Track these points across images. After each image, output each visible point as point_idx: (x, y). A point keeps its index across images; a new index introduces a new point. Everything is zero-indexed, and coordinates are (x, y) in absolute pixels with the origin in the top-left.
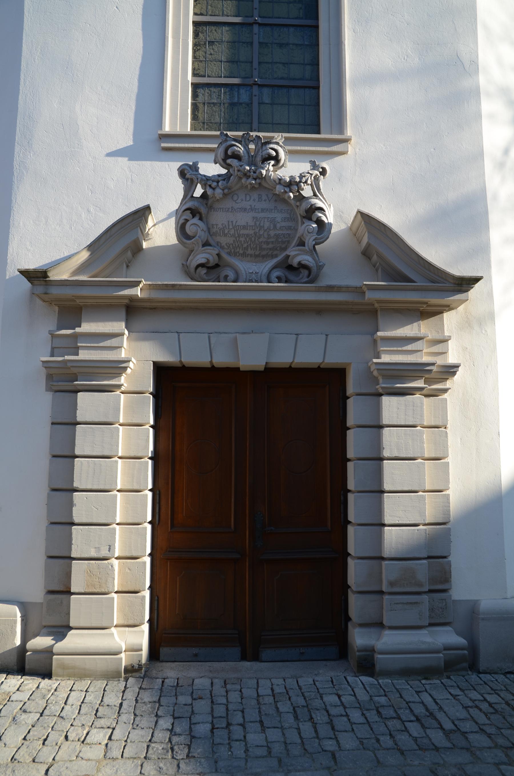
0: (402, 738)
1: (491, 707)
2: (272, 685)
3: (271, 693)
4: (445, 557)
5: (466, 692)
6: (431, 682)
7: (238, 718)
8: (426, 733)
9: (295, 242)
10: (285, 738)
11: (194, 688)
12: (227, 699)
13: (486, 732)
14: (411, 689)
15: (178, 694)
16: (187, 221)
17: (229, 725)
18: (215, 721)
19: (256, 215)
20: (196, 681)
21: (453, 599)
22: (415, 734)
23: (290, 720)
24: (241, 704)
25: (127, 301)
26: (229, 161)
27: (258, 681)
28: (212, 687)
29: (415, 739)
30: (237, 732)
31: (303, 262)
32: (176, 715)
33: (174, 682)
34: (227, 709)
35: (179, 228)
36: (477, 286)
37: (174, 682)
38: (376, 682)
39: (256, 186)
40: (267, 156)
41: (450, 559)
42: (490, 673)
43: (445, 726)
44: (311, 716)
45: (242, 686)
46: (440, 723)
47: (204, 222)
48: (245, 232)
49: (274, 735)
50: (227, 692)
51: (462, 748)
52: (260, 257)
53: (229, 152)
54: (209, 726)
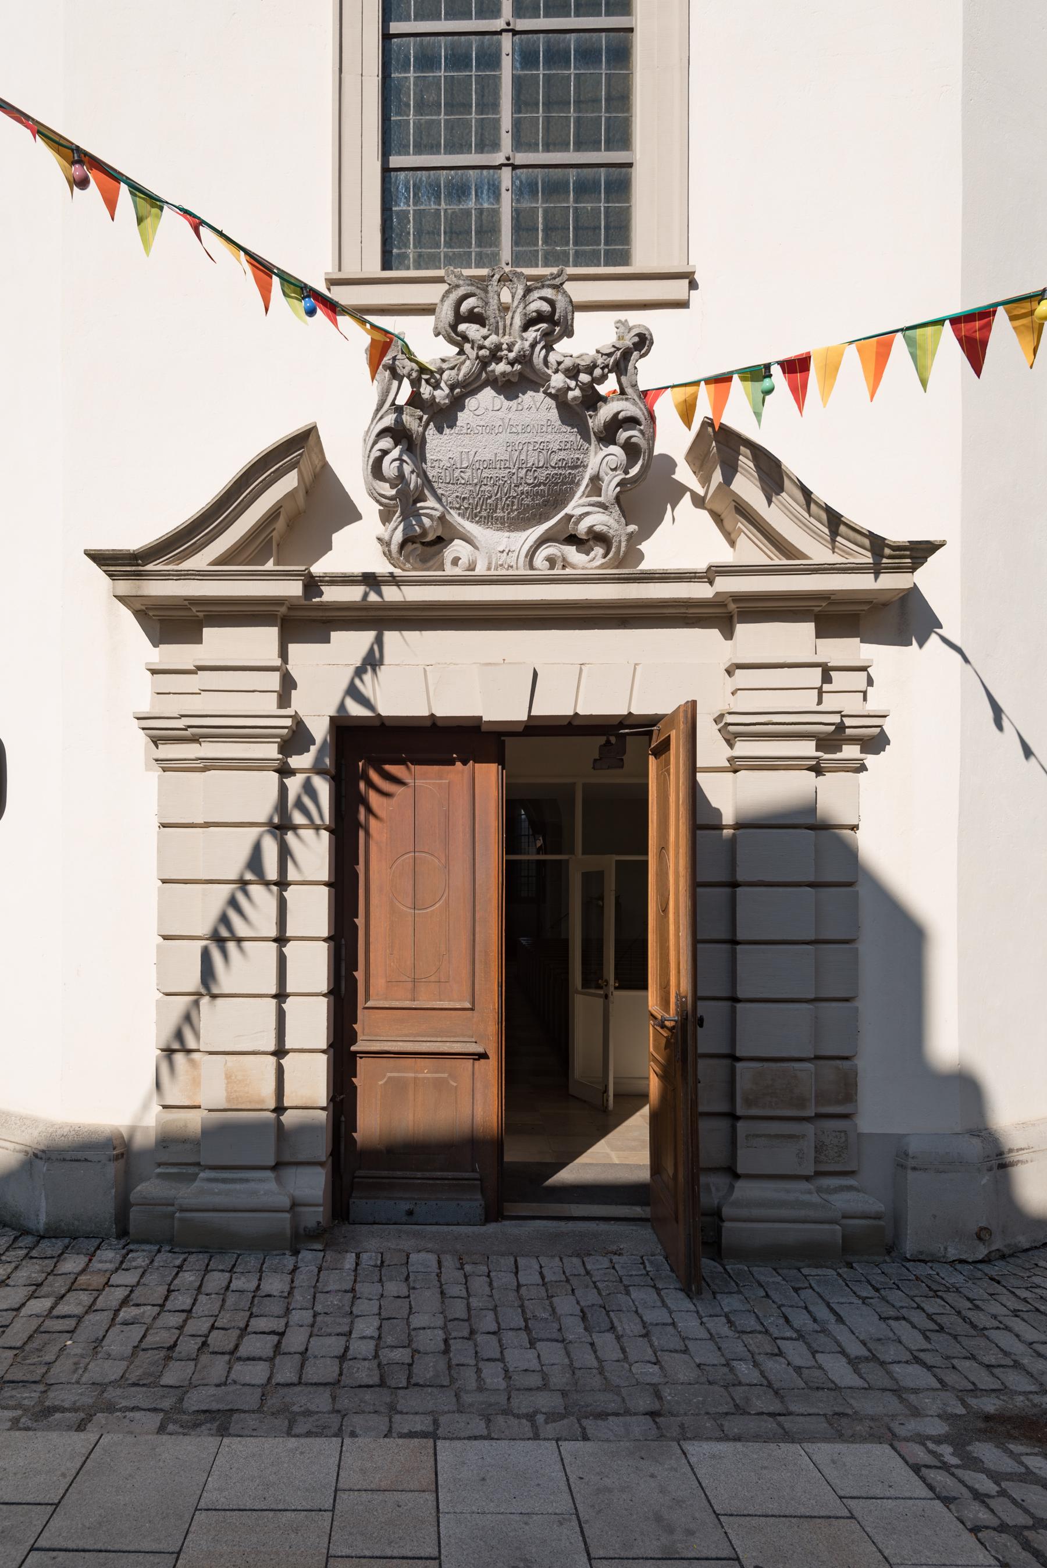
0: (774, 1367)
1: (932, 1320)
2: (541, 1267)
3: (540, 1281)
4: (846, 1058)
5: (882, 1292)
6: (819, 1271)
7: (488, 1323)
8: (816, 1361)
9: (582, 488)
10: (571, 1361)
11: (411, 1269)
12: (467, 1289)
13: (925, 1364)
14: (784, 1282)
15: (384, 1279)
16: (385, 452)
17: (472, 1332)
18: (450, 1325)
19: (513, 438)
20: (413, 1257)
21: (860, 1131)
22: (798, 1361)
23: (574, 1329)
24: (490, 1299)
25: (283, 610)
26: (462, 327)
27: (516, 1261)
28: (440, 1268)
29: (798, 1370)
30: (489, 1346)
31: (597, 528)
32: (384, 1315)
33: (377, 1259)
34: (468, 1305)
35: (370, 467)
36: (933, 560)
37: (377, 1259)
38: (720, 1269)
39: (512, 380)
40: (534, 314)
41: (856, 1061)
42: (925, 1262)
43: (848, 1351)
44: (612, 1322)
45: (491, 1267)
46: (838, 1343)
47: (416, 456)
48: (493, 473)
49: (552, 1353)
50: (466, 1277)
51: (884, 1390)
52: (520, 521)
53: (465, 307)
54: (440, 1334)
